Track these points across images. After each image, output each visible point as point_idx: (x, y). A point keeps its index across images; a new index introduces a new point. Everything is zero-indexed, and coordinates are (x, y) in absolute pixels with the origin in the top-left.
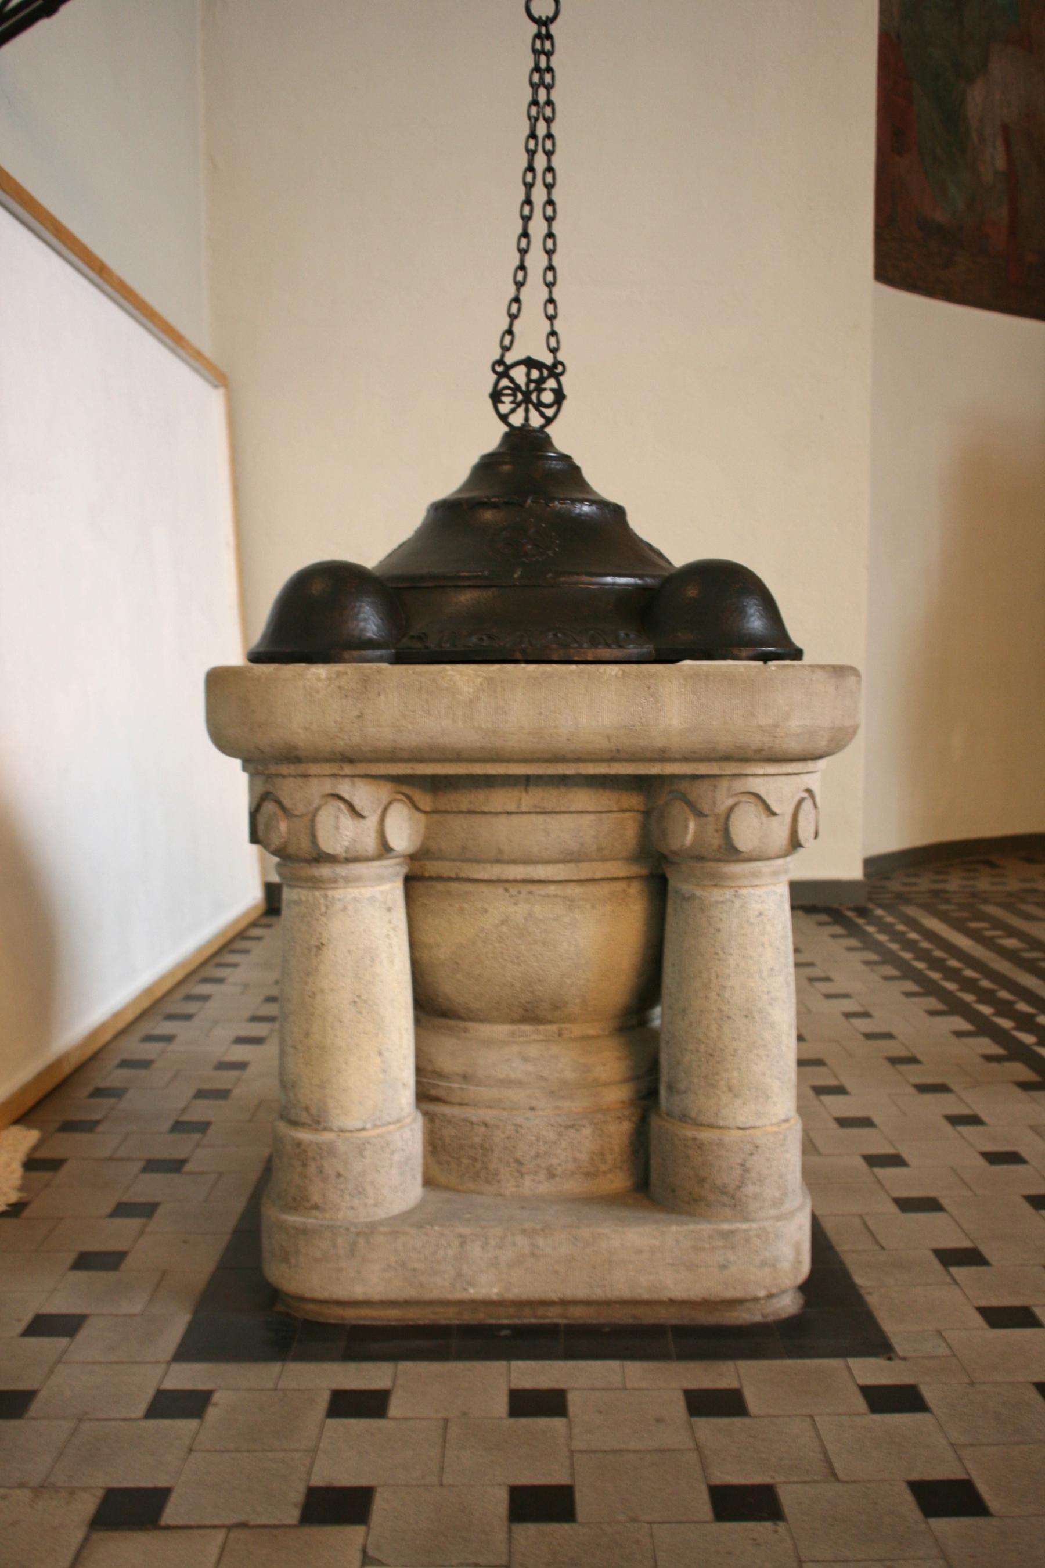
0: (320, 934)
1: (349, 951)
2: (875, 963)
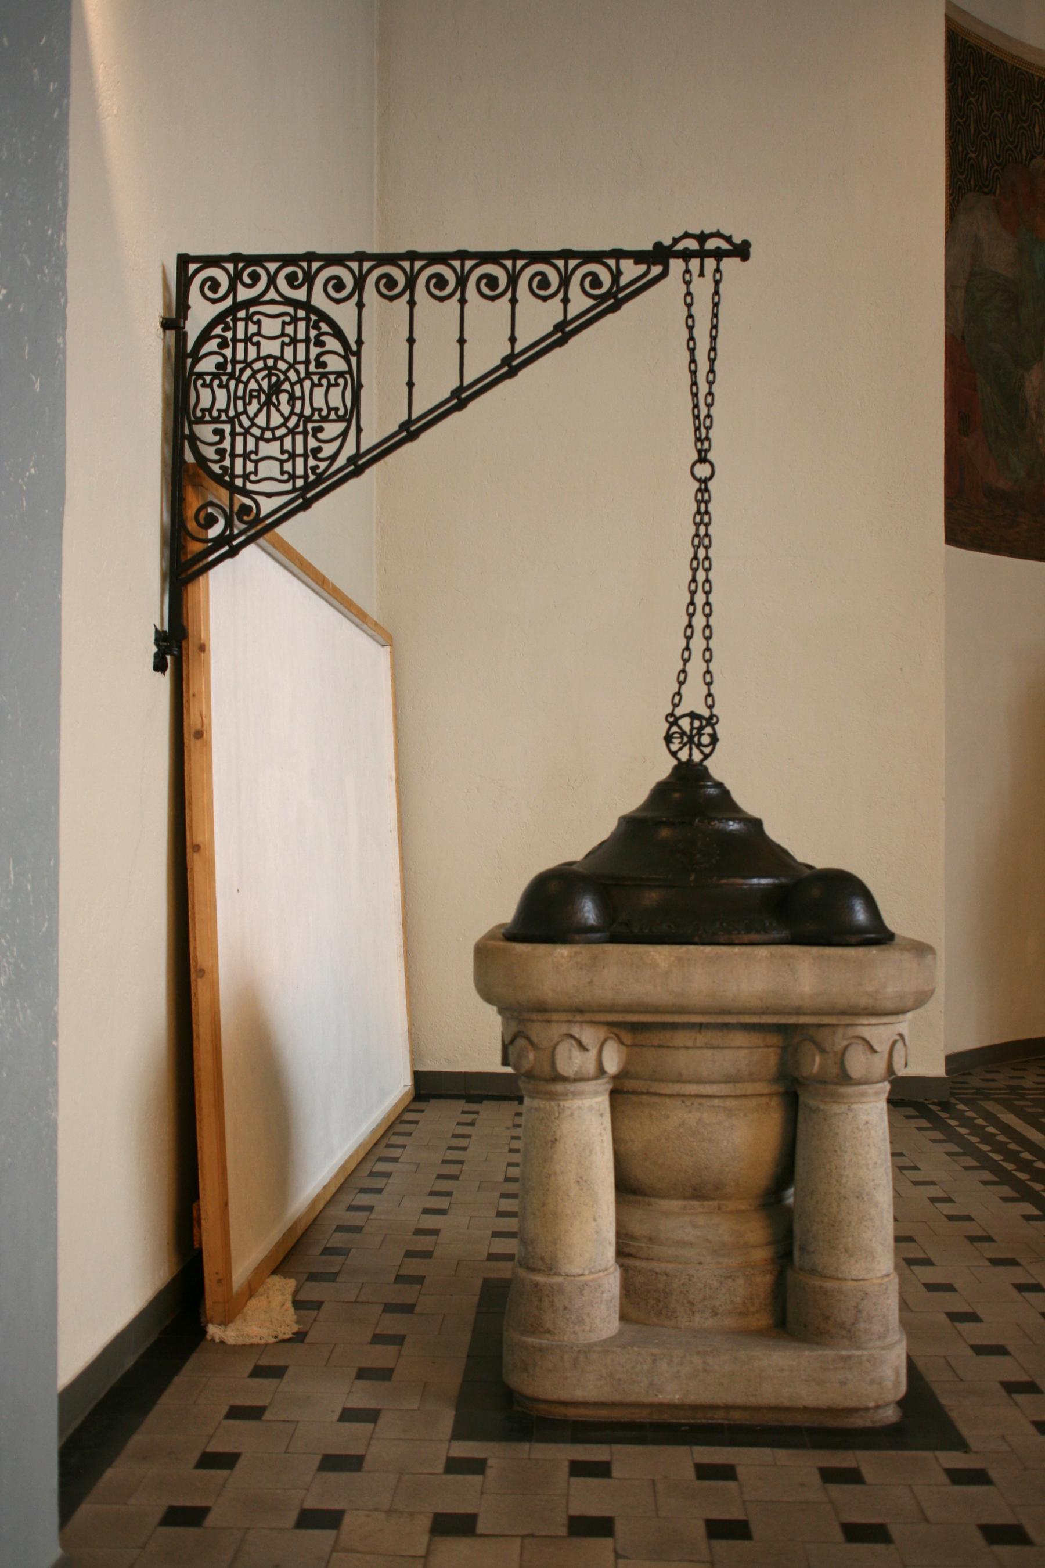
0: (554, 1132)
1: (575, 1145)
2: (957, 1154)
